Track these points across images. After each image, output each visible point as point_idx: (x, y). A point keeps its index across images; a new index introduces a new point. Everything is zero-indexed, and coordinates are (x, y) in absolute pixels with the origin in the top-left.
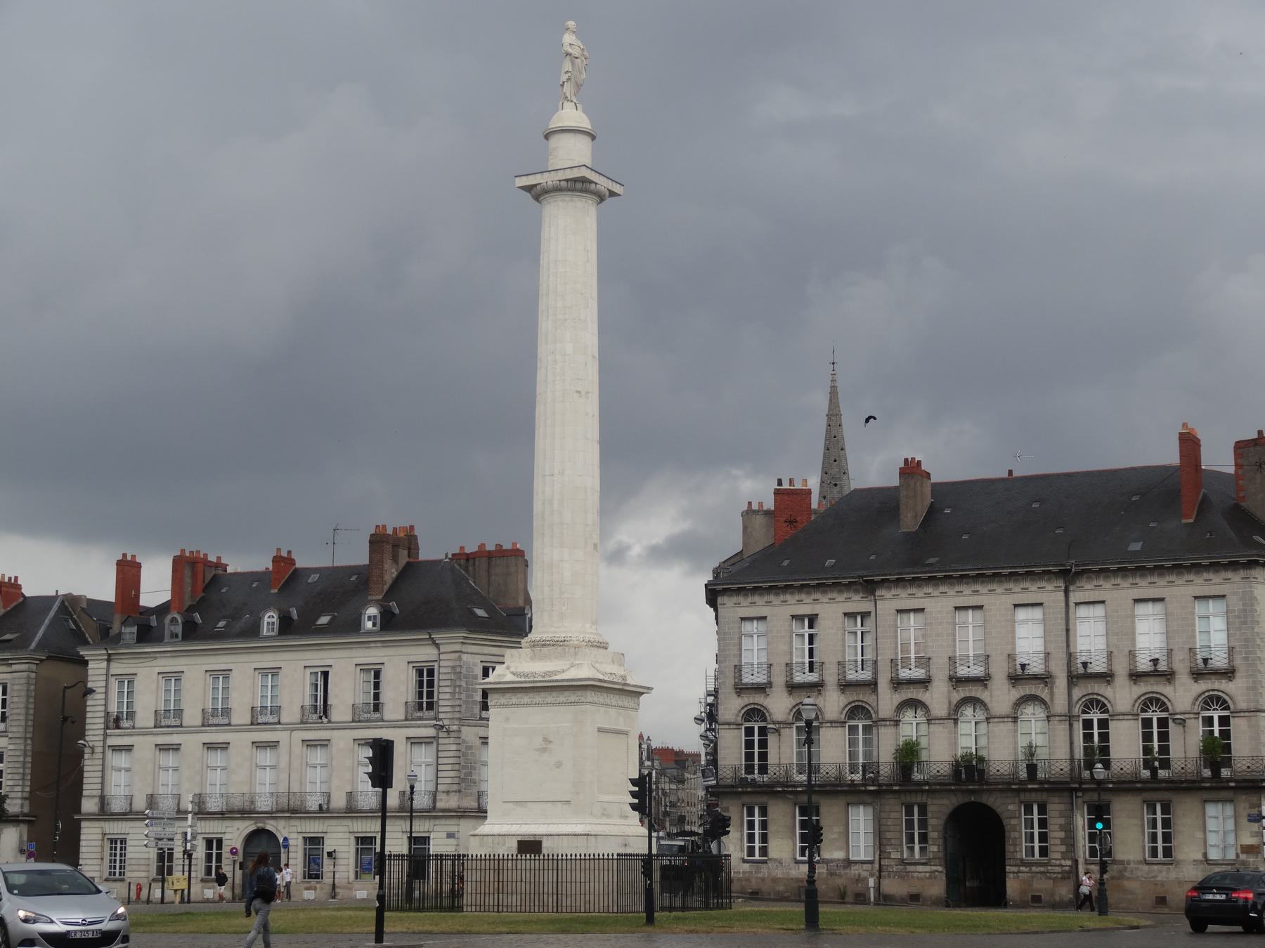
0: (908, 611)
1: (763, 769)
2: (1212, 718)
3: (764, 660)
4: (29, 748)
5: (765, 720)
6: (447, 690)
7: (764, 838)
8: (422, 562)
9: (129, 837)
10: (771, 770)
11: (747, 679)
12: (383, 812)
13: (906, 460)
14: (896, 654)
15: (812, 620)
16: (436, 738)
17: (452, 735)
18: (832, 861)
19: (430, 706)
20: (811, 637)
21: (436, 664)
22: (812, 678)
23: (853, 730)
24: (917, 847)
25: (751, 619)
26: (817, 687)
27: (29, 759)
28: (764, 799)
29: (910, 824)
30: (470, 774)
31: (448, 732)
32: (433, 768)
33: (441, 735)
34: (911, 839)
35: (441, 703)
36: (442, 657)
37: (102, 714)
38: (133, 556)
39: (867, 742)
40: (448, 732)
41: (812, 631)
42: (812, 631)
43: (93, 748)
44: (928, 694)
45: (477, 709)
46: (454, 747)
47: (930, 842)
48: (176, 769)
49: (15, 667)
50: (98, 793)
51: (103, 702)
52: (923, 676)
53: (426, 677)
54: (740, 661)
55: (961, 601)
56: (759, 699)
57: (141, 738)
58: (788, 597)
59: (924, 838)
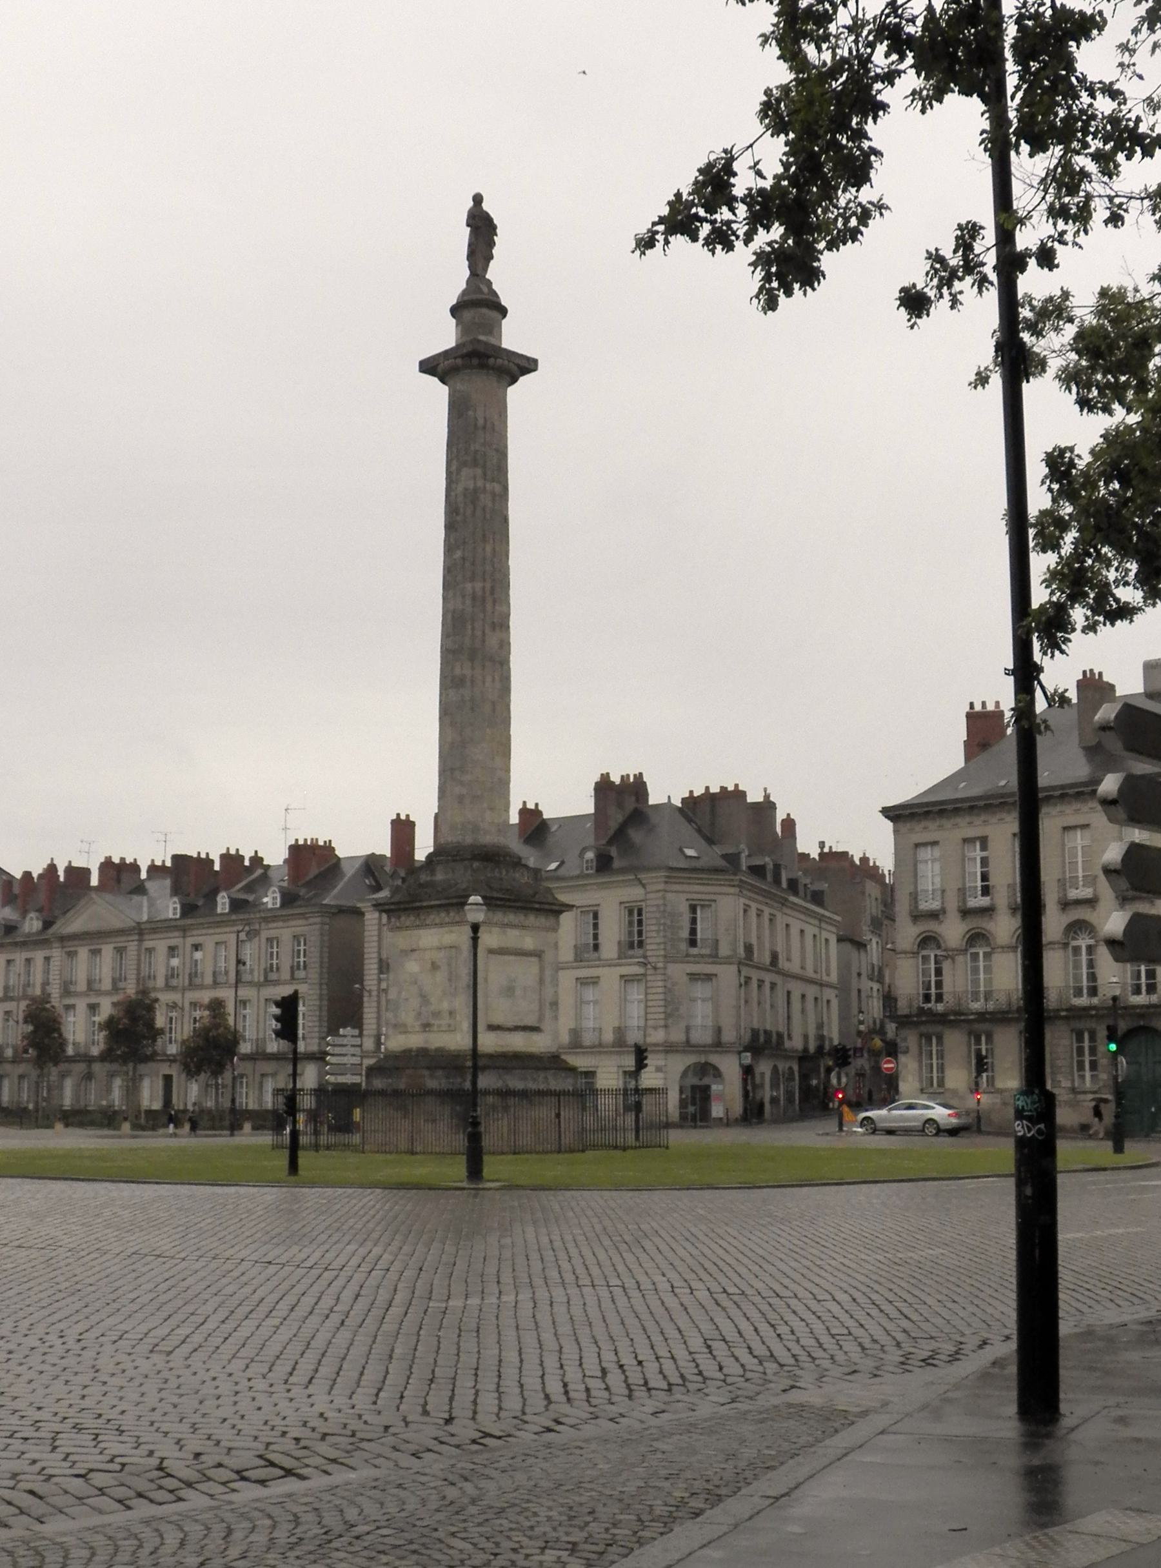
0: (1074, 828)
1: (939, 998)
2: (977, 954)
3: (938, 886)
4: (325, 992)
5: (939, 947)
6: (653, 928)
7: (941, 1069)
8: (657, 807)
9: (599, 1071)
10: (1101, 992)
11: (924, 906)
12: (296, 1059)
13: (1084, 672)
14: (1064, 872)
15: (984, 842)
16: (644, 975)
17: (658, 971)
18: (1005, 1090)
19: (641, 944)
20: (985, 862)
21: (643, 904)
22: (984, 901)
23: (975, 957)
24: (1088, 1074)
25: (925, 844)
26: (988, 911)
27: (325, 1003)
28: (938, 1028)
29: (1080, 1051)
30: (677, 1009)
31: (655, 968)
32: (642, 1005)
33: (649, 972)
34: (1081, 1067)
35: (648, 941)
36: (649, 896)
37: (376, 961)
38: (408, 816)
39: (988, 969)
40: (655, 968)
41: (984, 854)
42: (984, 854)
43: (370, 991)
44: (1095, 914)
45: (683, 946)
46: (660, 984)
47: (1100, 1068)
48: (596, 1002)
49: (312, 920)
50: (375, 1032)
51: (376, 950)
52: (1090, 896)
53: (635, 914)
54: (916, 887)
55: (1071, 820)
56: (932, 926)
57: (606, 969)
58: (959, 820)
59: (1094, 1066)
